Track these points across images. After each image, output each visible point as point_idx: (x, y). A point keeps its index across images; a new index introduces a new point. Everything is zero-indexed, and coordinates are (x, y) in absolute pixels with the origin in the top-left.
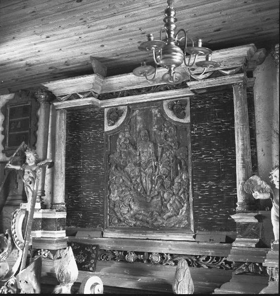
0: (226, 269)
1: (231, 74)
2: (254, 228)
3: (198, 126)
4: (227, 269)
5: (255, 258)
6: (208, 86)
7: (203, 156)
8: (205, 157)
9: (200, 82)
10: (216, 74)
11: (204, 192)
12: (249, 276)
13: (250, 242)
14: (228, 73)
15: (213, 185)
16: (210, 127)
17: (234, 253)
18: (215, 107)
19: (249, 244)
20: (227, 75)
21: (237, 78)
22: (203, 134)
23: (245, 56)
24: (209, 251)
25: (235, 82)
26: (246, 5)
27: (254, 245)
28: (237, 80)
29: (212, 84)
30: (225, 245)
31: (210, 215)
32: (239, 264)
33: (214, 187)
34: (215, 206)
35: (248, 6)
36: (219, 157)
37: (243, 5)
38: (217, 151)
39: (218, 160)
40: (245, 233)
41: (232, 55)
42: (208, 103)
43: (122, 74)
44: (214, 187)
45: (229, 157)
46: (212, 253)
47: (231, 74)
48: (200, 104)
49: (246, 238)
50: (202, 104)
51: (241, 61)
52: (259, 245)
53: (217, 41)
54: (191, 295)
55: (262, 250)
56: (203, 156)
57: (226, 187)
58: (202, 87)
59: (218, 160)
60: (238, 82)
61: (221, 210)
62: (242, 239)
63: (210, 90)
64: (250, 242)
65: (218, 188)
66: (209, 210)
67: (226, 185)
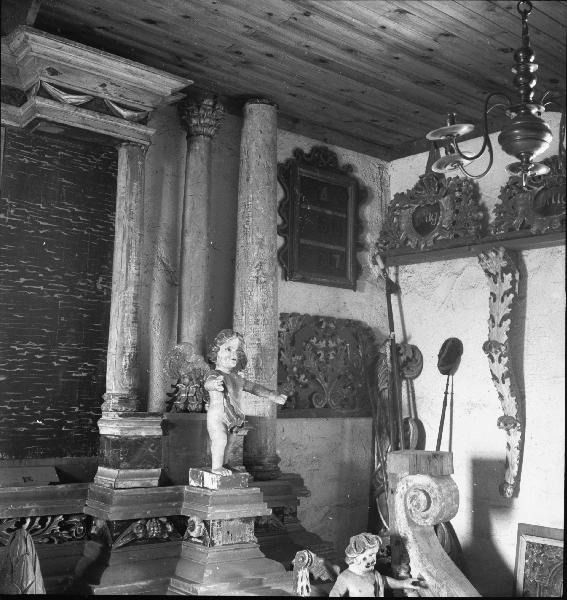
0: (59, 543)
1: (131, 120)
2: (153, 448)
3: (18, 206)
4: (61, 540)
5: (160, 508)
6: (78, 125)
7: (22, 280)
8: (25, 283)
9: (66, 108)
10: (96, 105)
11: (13, 365)
12: (143, 547)
13: (147, 476)
14: (125, 113)
15: (40, 353)
16: (46, 216)
17: (121, 503)
18: (64, 175)
19: (147, 480)
20: (121, 117)
21: (141, 133)
22: (26, 227)
23: (163, 97)
24: (28, 507)
25: (137, 141)
26: (269, 20)
27: (155, 482)
28: (138, 136)
29: (90, 123)
30: (60, 487)
31: (21, 421)
32: (125, 524)
33: (38, 357)
34: (36, 400)
35: (270, 24)
36: (58, 288)
37: (261, 17)
38: (54, 273)
39: (56, 296)
40: (137, 457)
41: (144, 81)
42: (46, 159)
43: (88, 44)
44: (38, 357)
45: (80, 293)
46: (37, 510)
47: (131, 120)
48: (29, 155)
49: (136, 468)
50: (34, 156)
51: (152, 102)
52: (165, 481)
53: (119, 38)
54: (316, 598)
55: (169, 490)
56: (22, 280)
57: (66, 359)
58: (62, 122)
59: (56, 296)
60: (141, 142)
61: (48, 409)
62: (132, 471)
63: (71, 133)
64: (147, 476)
65: (48, 360)
66: (22, 410)
67: (66, 354)
